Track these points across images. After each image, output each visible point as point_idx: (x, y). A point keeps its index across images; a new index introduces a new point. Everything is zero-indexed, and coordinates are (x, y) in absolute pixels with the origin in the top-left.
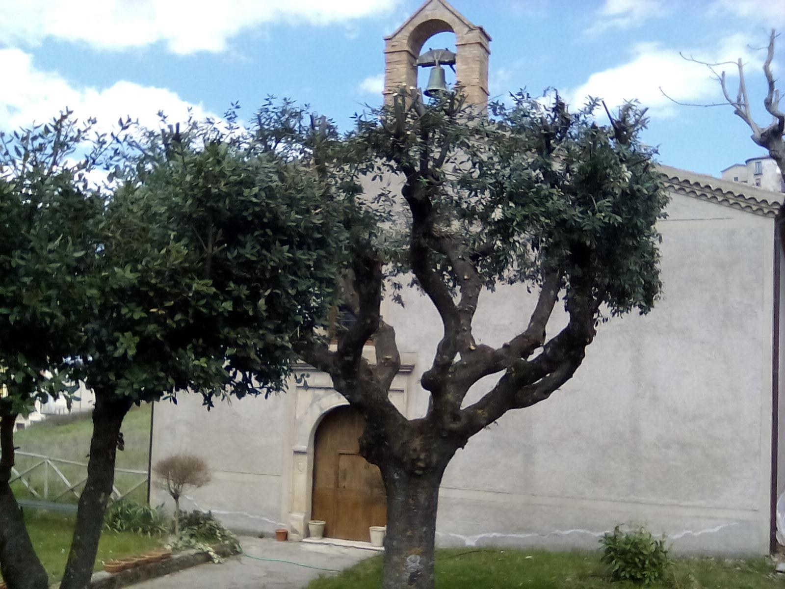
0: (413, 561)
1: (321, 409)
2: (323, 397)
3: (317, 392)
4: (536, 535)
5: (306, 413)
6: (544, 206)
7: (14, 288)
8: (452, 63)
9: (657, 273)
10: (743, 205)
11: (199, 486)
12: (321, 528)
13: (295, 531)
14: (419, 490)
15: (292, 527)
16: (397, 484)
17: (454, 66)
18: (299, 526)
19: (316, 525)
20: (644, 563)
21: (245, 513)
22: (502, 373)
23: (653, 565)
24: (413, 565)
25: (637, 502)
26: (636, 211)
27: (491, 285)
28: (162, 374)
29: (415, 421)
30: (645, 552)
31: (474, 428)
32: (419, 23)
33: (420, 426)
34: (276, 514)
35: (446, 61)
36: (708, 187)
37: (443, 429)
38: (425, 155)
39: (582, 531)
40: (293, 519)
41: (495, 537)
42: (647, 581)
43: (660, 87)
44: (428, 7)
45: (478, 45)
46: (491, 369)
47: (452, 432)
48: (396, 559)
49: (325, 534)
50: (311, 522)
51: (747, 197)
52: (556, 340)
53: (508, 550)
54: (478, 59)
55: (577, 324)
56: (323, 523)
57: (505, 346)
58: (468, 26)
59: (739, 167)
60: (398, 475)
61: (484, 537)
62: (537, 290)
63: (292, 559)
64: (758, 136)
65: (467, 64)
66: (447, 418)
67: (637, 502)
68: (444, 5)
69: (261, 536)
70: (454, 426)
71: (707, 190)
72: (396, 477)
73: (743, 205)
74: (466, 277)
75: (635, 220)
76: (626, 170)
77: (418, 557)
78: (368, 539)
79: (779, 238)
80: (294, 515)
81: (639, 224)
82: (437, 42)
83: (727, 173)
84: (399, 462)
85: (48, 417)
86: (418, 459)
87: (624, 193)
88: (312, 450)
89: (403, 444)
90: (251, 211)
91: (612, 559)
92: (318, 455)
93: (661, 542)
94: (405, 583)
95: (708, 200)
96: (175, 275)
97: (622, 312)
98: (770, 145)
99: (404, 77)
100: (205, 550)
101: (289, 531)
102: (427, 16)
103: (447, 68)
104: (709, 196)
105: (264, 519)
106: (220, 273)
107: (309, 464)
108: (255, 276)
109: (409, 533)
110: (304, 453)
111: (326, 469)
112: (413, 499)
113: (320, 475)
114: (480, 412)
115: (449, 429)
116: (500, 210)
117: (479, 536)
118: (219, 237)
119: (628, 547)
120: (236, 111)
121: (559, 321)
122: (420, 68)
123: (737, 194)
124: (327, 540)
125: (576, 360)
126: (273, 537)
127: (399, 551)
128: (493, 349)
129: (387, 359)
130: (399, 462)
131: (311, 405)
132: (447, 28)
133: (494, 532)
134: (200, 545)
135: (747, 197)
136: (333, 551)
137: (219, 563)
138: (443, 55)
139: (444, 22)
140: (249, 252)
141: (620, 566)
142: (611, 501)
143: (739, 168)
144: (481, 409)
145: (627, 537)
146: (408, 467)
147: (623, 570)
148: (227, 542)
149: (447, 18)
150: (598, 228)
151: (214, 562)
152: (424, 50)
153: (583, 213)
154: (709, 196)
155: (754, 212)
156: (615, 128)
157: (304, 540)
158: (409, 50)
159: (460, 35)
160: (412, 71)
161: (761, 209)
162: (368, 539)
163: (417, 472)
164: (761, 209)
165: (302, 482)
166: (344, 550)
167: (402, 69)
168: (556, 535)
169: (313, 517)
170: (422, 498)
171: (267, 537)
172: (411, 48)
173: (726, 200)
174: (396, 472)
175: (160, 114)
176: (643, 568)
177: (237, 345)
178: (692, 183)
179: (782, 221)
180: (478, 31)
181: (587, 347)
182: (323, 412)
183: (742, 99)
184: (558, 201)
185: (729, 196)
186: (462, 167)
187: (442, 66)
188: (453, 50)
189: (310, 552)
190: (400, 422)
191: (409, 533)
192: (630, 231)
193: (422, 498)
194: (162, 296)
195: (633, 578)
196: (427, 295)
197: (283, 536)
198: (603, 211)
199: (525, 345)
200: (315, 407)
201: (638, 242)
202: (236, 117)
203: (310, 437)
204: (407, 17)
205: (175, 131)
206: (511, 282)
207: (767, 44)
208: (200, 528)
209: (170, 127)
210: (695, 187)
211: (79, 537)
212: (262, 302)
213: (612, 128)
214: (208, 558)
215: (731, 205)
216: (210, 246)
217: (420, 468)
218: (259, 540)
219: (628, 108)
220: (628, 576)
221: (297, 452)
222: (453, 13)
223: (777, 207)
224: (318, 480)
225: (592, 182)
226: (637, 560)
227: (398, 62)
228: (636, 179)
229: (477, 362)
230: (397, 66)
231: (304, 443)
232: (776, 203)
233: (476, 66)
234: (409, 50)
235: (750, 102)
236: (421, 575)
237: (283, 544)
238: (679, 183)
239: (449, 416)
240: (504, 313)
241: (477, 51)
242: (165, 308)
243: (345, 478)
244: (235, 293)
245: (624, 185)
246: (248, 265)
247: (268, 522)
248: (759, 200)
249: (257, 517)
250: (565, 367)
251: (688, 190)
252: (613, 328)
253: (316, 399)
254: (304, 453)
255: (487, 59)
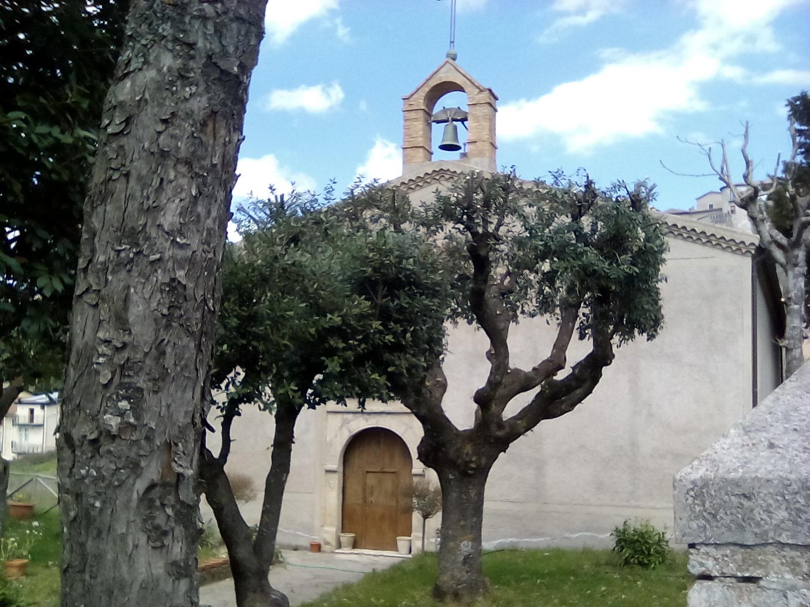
0: (466, 546)
1: (350, 431)
2: (352, 420)
3: (346, 416)
4: (548, 538)
5: (336, 436)
6: (580, 260)
7: (262, 328)
8: (463, 120)
9: (660, 308)
10: (724, 246)
11: (247, 502)
12: (352, 539)
13: (327, 543)
14: (471, 487)
15: (325, 539)
16: (452, 483)
17: (465, 123)
18: (332, 540)
19: (347, 537)
20: (649, 550)
22: (538, 389)
23: (657, 552)
24: (466, 549)
25: (638, 507)
26: (648, 262)
27: (515, 318)
28: (349, 385)
29: (465, 431)
30: (650, 542)
31: (514, 436)
32: (435, 84)
33: (469, 436)
34: (309, 529)
35: (459, 118)
36: (693, 230)
37: (490, 436)
38: (486, 222)
39: (589, 534)
40: (326, 532)
41: (511, 542)
42: (653, 566)
43: (661, 161)
44: (443, 70)
45: (487, 105)
46: (525, 388)
47: (498, 439)
48: (451, 544)
49: (355, 545)
50: (342, 534)
51: (728, 239)
52: (583, 363)
53: (528, 549)
54: (487, 117)
56: (353, 535)
57: (534, 369)
58: (478, 88)
59: (713, 195)
60: (453, 475)
61: (500, 543)
62: (554, 322)
63: (330, 566)
64: (738, 200)
65: (478, 122)
66: (493, 427)
67: (638, 507)
68: (455, 68)
70: (500, 433)
71: (693, 233)
72: (451, 477)
73: (724, 246)
74: (498, 312)
75: (647, 269)
76: (641, 232)
77: (470, 543)
78: (395, 548)
79: (755, 274)
80: (326, 528)
81: (650, 272)
82: (449, 101)
83: (702, 200)
84: (453, 464)
85: (20, 457)
86: (471, 462)
87: (640, 249)
88: (341, 469)
89: (457, 450)
90: (403, 274)
91: (622, 548)
92: (347, 474)
93: (663, 533)
94: (459, 565)
95: (694, 241)
96: (361, 317)
97: (628, 340)
98: (749, 208)
99: (421, 133)
101: (322, 544)
102: (440, 78)
103: (459, 124)
104: (695, 238)
106: (384, 315)
107: (339, 481)
108: (407, 318)
109: (462, 523)
110: (334, 472)
111: (355, 487)
112: (466, 495)
113: (349, 491)
114: (519, 422)
115: (493, 436)
116: (548, 264)
117: (496, 542)
118: (385, 292)
119: (636, 538)
120: (334, 186)
121: (579, 350)
122: (434, 124)
123: (719, 236)
124: (357, 551)
125: (595, 379)
127: (454, 538)
128: (525, 372)
129: (439, 381)
130: (453, 464)
132: (460, 89)
133: (510, 537)
135: (728, 239)
136: (364, 559)
138: (455, 114)
139: (456, 83)
140: (404, 301)
141: (630, 554)
142: (614, 506)
143: (714, 195)
144: (520, 419)
145: (634, 530)
146: (462, 467)
147: (632, 557)
149: (459, 80)
150: (622, 276)
152: (437, 108)
153: (610, 264)
154: (695, 238)
155: (733, 252)
156: (632, 200)
157: (337, 551)
158: (426, 109)
159: (471, 96)
160: (427, 128)
161: (739, 249)
162: (395, 548)
163: (470, 472)
164: (739, 249)
165: (333, 498)
166: (375, 558)
167: (420, 125)
168: (566, 538)
169: (344, 529)
170: (473, 493)
171: (301, 550)
172: (427, 106)
173: (709, 242)
174: (451, 473)
175: (271, 188)
176: (649, 555)
177: (394, 365)
178: (679, 226)
179: (758, 259)
180: (487, 92)
181: (604, 369)
182: (352, 434)
183: (725, 169)
184: (592, 256)
185: (712, 238)
186: (513, 229)
187: (455, 123)
188: (465, 109)
189: (344, 561)
191: (462, 523)
192: (644, 278)
193: (473, 493)
194: (355, 332)
195: (641, 564)
196: (482, 331)
197: (317, 548)
198: (625, 265)
199: (551, 368)
201: (649, 286)
202: (333, 190)
203: (340, 457)
205: (279, 200)
206: (533, 316)
207: (743, 132)
209: (276, 197)
210: (682, 231)
211: (268, 506)
212: (408, 335)
213: (629, 200)
215: (714, 246)
216: (379, 297)
217: (472, 469)
218: (294, 552)
219: (639, 185)
220: (636, 562)
221: (328, 471)
222: (464, 76)
223: (754, 247)
224: (347, 496)
225: (614, 243)
226: (644, 548)
227: (416, 119)
228: (647, 239)
229: (513, 383)
230: (415, 123)
231: (335, 463)
232: (753, 244)
233: (486, 124)
234: (426, 109)
235: (731, 173)
237: (317, 555)
238: (669, 227)
240: (531, 340)
241: (487, 110)
242: (357, 340)
243: (372, 494)
244: (394, 330)
245: (640, 244)
246: (401, 310)
247: (302, 536)
248: (738, 241)
249: (292, 531)
250: (586, 385)
251: (676, 233)
252: (629, 352)
253: (345, 422)
254: (334, 472)
255: (494, 116)
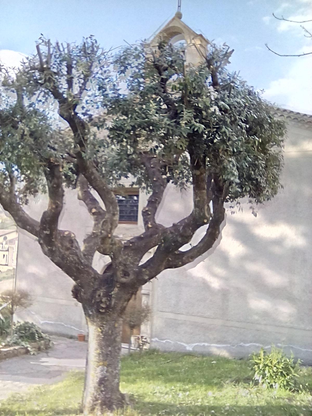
1: (105, 262)
4: (229, 345)
21: (63, 323)
37: (117, 282)
43: (266, 45)
55: (197, 209)
60: (92, 312)
69: (71, 337)
86: (101, 302)
100: (26, 346)
105: (73, 327)
114: (144, 270)
126: (77, 339)
131: (99, 260)
134: (23, 343)
137: (34, 354)
142: (276, 326)
144: (145, 268)
148: (42, 342)
151: (30, 355)
190: (92, 276)
200: (101, 261)
204: (158, 27)
208: (26, 332)
214: (27, 352)
217: (103, 308)
236: (108, 380)
239: (121, 272)
249: (69, 326)
